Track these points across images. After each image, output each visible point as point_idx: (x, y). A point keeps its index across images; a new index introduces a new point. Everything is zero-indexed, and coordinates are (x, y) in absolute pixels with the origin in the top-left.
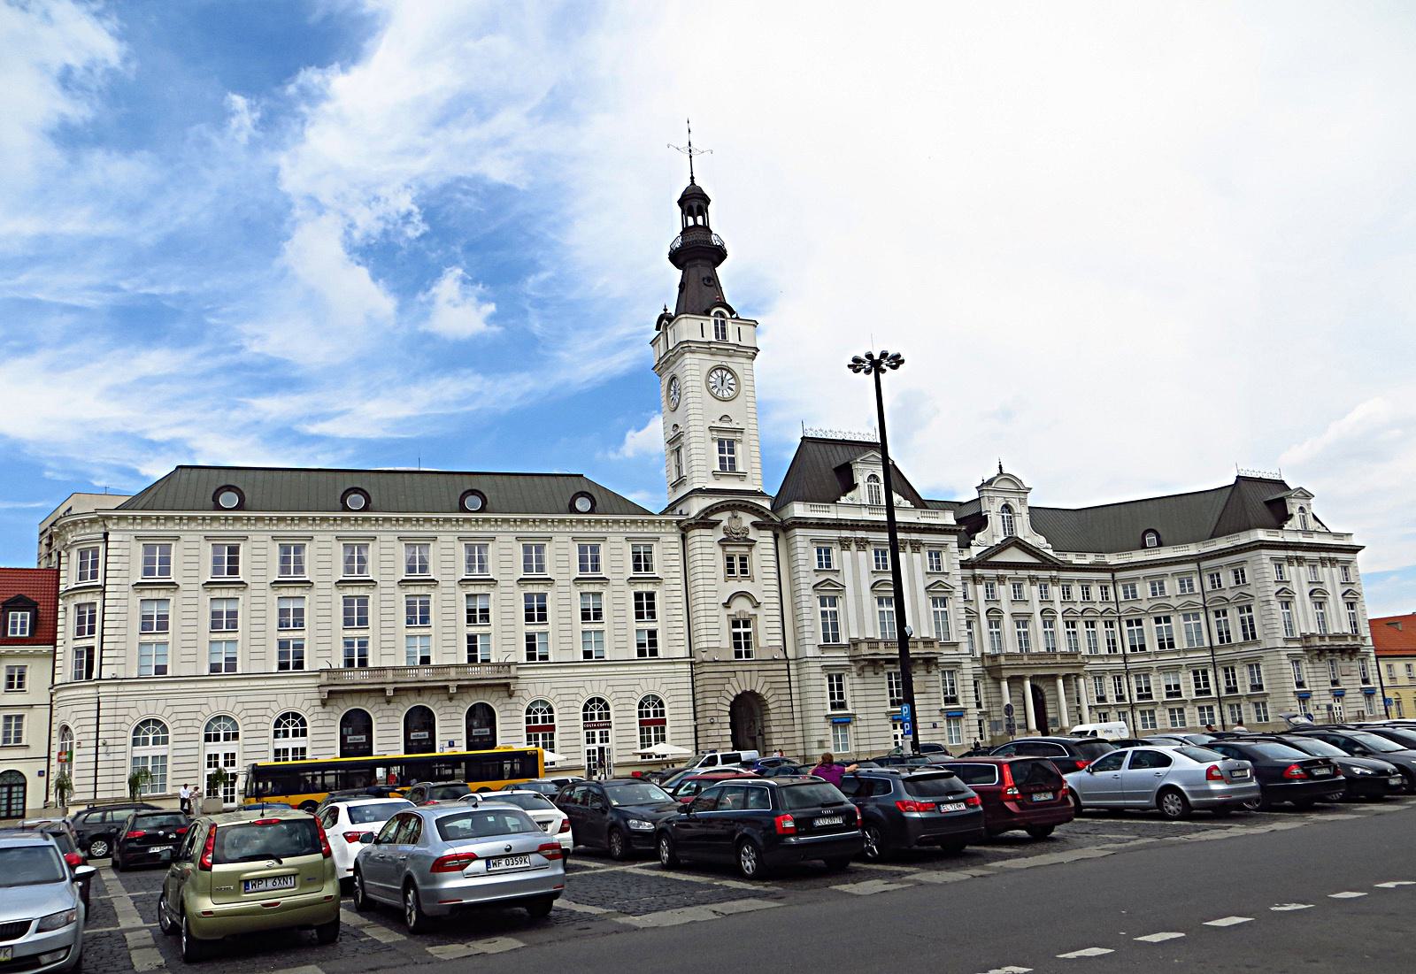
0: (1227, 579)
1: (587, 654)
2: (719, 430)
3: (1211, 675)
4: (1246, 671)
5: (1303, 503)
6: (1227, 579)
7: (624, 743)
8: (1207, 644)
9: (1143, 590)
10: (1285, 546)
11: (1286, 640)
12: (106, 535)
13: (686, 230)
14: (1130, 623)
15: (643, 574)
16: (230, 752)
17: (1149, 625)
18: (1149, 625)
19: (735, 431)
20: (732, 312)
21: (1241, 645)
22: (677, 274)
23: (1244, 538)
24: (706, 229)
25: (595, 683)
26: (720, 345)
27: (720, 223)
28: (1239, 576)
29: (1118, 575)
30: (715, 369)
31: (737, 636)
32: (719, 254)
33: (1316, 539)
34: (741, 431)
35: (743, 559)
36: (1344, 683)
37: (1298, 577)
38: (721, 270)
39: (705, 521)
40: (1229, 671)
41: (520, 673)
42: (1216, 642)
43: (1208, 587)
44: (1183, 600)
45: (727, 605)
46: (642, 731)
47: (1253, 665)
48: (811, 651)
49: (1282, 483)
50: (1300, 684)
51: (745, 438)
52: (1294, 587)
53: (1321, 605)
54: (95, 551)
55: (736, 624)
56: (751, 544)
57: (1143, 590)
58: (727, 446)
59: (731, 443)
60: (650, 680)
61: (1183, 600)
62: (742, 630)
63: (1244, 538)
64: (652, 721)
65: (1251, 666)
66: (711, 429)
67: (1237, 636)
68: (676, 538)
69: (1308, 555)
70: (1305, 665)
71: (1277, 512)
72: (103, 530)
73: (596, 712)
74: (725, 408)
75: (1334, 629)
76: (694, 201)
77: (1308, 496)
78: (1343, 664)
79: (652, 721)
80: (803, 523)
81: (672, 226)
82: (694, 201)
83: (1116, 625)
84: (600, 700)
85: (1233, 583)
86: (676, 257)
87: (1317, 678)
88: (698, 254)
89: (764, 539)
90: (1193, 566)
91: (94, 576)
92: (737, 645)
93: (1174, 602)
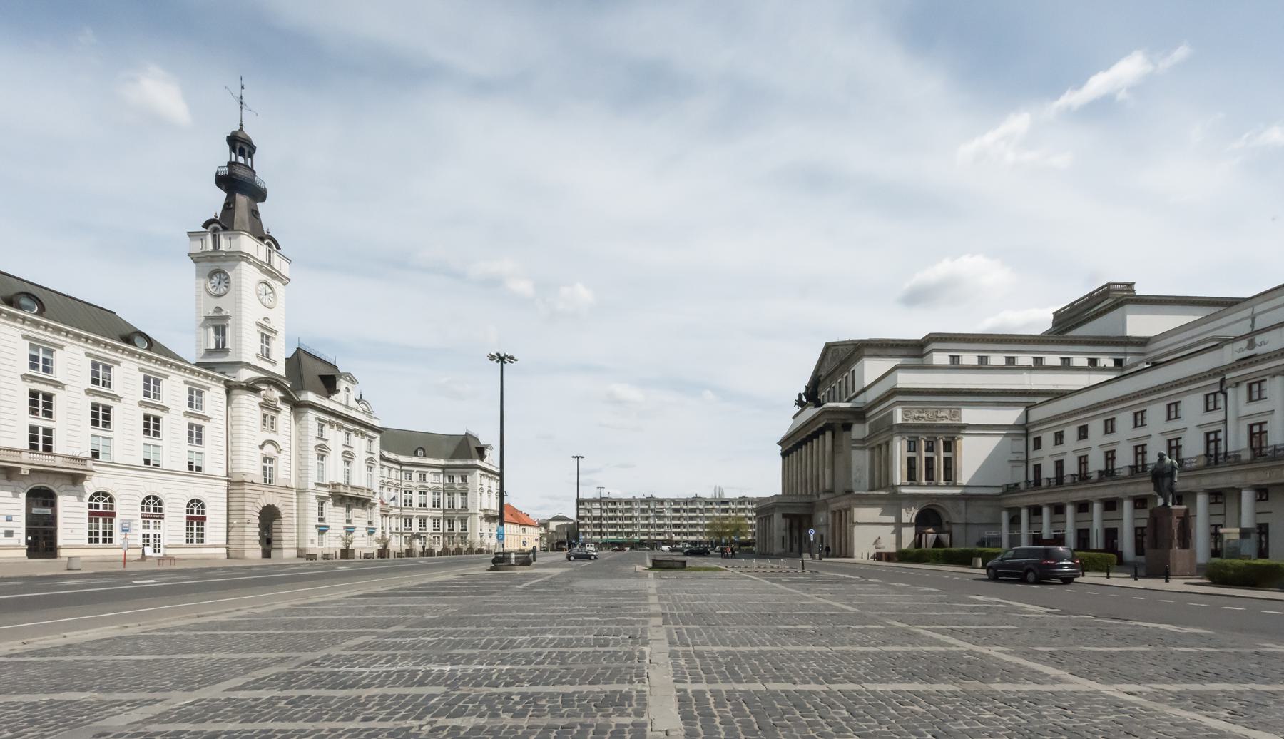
1: (147, 462)
5: (350, 386)
7: (173, 530)
9: (415, 476)
10: (331, 413)
11: (318, 485)
15: (100, 388)
17: (415, 494)
18: (415, 494)
20: (278, 247)
25: (153, 484)
26: (268, 269)
27: (264, 167)
28: (464, 478)
31: (265, 468)
33: (354, 414)
35: (273, 418)
36: (355, 523)
37: (335, 438)
39: (252, 388)
40: (451, 522)
41: (95, 468)
45: (261, 447)
46: (90, 520)
48: (311, 486)
49: (336, 367)
50: (321, 520)
52: (355, 451)
53: (348, 463)
55: (265, 460)
56: (278, 411)
57: (415, 476)
58: (266, 339)
59: (268, 337)
60: (196, 488)
62: (268, 465)
63: (469, 462)
64: (196, 519)
66: (258, 324)
68: (223, 391)
69: (346, 425)
70: (329, 505)
71: (329, 383)
73: (153, 507)
74: (267, 313)
75: (353, 482)
77: (353, 381)
78: (356, 511)
79: (196, 519)
80: (312, 406)
87: (336, 516)
89: (286, 409)
92: (265, 475)
93: (430, 485)
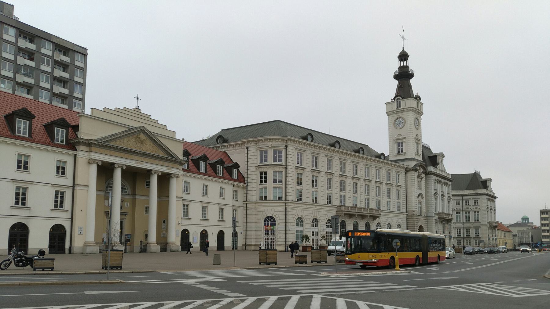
0: (472, 202)
2: (397, 140)
3: (462, 230)
4: (474, 230)
6: (472, 202)
8: (462, 221)
12: (286, 146)
13: (400, 68)
14: (466, 213)
16: (319, 224)
19: (402, 139)
21: (473, 223)
22: (397, 82)
23: (480, 191)
24: (407, 67)
27: (412, 64)
28: (476, 202)
29: (464, 197)
30: (397, 119)
32: (412, 75)
34: (405, 138)
38: (412, 81)
40: (468, 230)
42: (465, 221)
43: (464, 204)
44: (475, 207)
47: (477, 229)
51: (406, 140)
54: (281, 152)
61: (475, 207)
65: (476, 229)
67: (472, 219)
72: (285, 144)
74: (399, 132)
76: (403, 57)
81: (395, 66)
82: (403, 57)
83: (461, 213)
84: (272, 217)
85: (474, 204)
86: (396, 77)
88: (404, 76)
90: (461, 198)
91: (280, 160)
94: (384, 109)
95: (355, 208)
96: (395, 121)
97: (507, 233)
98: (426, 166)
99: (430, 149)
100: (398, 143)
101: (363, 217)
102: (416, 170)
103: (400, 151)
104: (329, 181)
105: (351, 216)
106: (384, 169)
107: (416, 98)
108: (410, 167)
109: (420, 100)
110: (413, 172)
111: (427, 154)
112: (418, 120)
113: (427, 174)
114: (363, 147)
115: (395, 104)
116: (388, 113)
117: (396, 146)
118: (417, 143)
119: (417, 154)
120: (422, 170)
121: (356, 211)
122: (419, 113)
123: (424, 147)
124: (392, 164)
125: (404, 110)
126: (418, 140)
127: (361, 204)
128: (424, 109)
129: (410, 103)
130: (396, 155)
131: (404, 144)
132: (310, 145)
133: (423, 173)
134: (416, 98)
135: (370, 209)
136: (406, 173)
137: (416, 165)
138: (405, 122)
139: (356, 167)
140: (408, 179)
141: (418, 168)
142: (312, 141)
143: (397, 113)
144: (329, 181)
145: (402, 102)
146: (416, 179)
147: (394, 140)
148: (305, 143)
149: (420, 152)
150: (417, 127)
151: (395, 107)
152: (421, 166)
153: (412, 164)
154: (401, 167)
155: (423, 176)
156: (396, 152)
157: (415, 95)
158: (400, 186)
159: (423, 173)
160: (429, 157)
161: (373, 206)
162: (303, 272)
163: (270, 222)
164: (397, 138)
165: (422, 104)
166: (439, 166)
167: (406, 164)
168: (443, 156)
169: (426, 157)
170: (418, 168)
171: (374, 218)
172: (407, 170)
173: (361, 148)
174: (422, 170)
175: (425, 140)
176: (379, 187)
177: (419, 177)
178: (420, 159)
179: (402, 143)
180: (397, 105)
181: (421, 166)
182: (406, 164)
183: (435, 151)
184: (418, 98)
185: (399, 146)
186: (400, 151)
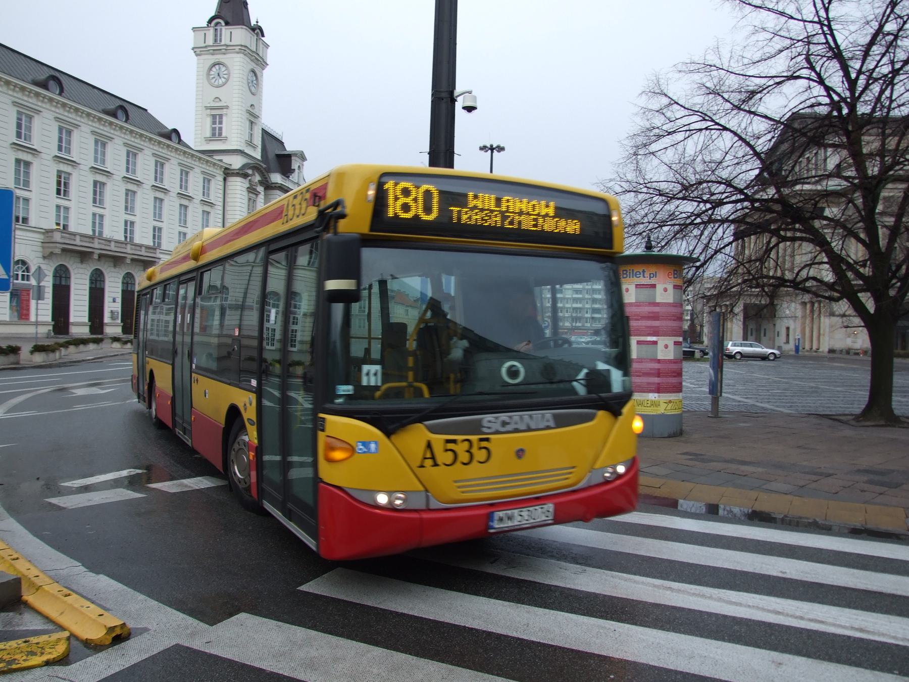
2: (212, 108)
19: (221, 108)
30: (214, 65)
34: (227, 107)
82: (481, 149)
94: (190, 40)
95: (155, 249)
96: (210, 69)
97: (410, 309)
98: (269, 170)
99: (282, 143)
100: (214, 116)
101: (116, 260)
102: (245, 176)
103: (217, 134)
104: (98, 187)
105: (84, 256)
106: (197, 170)
107: (253, 29)
108: (233, 167)
109: (263, 36)
110: (239, 179)
111: (274, 150)
112: (256, 75)
113: (269, 187)
114: (127, 107)
115: (211, 33)
116: (198, 51)
117: (209, 121)
118: (252, 123)
119: (250, 143)
120: (257, 178)
121: (96, 245)
122: (258, 61)
123: (265, 133)
124: (200, 159)
125: (227, 49)
126: (253, 117)
127: (113, 230)
128: (271, 56)
129: (238, 35)
130: (208, 140)
131: (224, 119)
132: (121, 128)
133: (261, 183)
134: (253, 29)
135: (136, 245)
136: (225, 179)
137: (244, 166)
138: (229, 74)
139: (160, 165)
140: (228, 192)
141: (250, 172)
142: (126, 121)
143: (215, 52)
144: (98, 187)
145: (225, 31)
146: (246, 193)
147: (207, 108)
148: (111, 124)
149: (258, 141)
150: (253, 89)
151: (210, 41)
152: (256, 168)
153: (236, 162)
154: (214, 164)
155: (260, 189)
156: (208, 134)
157: (253, 23)
158: (211, 204)
159: (261, 183)
160: (278, 156)
161: (142, 236)
162: (57, 377)
163: (20, 273)
164: (213, 104)
165: (267, 46)
166: (294, 177)
167: (228, 160)
168: (303, 158)
169: (271, 156)
170: (250, 172)
171: (146, 264)
172: (228, 173)
173: (122, 107)
174: (257, 178)
175: (270, 120)
176: (186, 207)
177: (251, 190)
178: (258, 155)
179: (221, 116)
180: (216, 35)
181: (256, 168)
182: (228, 160)
183: (290, 147)
184: (258, 31)
185: (214, 123)
186: (217, 134)
